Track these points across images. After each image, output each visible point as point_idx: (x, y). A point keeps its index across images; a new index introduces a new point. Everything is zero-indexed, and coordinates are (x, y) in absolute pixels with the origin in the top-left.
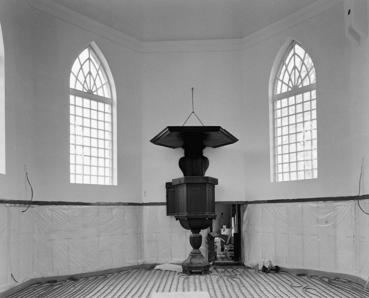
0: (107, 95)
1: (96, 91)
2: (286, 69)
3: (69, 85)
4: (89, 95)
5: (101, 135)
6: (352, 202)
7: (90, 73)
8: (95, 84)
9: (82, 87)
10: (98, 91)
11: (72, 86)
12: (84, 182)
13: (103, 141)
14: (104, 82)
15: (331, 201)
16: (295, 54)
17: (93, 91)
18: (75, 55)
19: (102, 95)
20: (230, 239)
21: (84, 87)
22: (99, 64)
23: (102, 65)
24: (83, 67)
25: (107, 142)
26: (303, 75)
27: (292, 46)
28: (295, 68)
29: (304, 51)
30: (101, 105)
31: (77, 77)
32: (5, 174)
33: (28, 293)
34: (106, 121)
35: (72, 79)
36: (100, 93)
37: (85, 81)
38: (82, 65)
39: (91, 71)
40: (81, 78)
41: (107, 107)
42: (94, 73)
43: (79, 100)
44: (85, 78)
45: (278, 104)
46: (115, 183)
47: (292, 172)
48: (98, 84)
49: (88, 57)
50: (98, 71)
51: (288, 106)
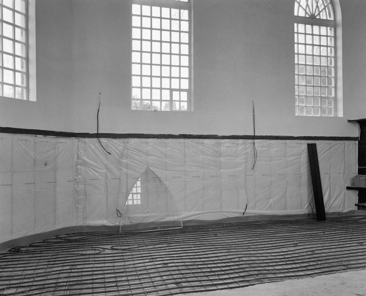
1: (319, 14)
6: (73, 139)
8: (317, 7)
10: (321, 14)
12: (4, 95)
15: (52, 137)
17: (316, 15)
19: (325, 18)
20: (271, 204)
25: (18, 45)
30: (324, 30)
33: (310, 235)
36: (323, 16)
37: (307, 5)
43: (300, 28)
46: (33, 98)
47: (151, 79)
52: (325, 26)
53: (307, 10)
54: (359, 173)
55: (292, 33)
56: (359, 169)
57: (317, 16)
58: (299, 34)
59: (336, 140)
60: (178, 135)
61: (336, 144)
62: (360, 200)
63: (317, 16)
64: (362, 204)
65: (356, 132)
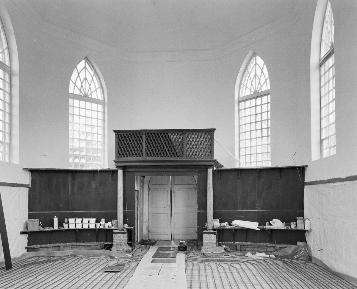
0: (100, 97)
1: (91, 94)
2: (249, 76)
3: (69, 91)
4: (85, 98)
5: (95, 122)
7: (86, 79)
8: (90, 89)
9: (79, 91)
11: (71, 91)
13: (96, 119)
14: (97, 86)
16: (256, 64)
18: (74, 66)
21: (81, 92)
22: (94, 71)
23: (96, 72)
24: (76, 84)
26: (262, 82)
27: (255, 55)
28: (256, 75)
29: (263, 62)
30: (95, 106)
31: (75, 84)
32: (19, 164)
34: (99, 110)
35: (71, 85)
36: (94, 96)
37: (82, 86)
38: (79, 74)
39: (86, 77)
40: (79, 84)
41: (100, 106)
42: (89, 79)
43: (76, 102)
44: (82, 83)
45: (242, 104)
48: (93, 89)
49: (84, 66)
50: (92, 77)
51: (256, 106)
52: (101, 104)
53: (82, 90)
54: (28, 219)
55: (67, 106)
56: (29, 214)
57: (89, 95)
58: (98, 112)
59: (14, 186)
60: (345, 177)
61: (15, 191)
62: (29, 243)
63: (89, 95)
64: (32, 246)
65: (27, 179)
